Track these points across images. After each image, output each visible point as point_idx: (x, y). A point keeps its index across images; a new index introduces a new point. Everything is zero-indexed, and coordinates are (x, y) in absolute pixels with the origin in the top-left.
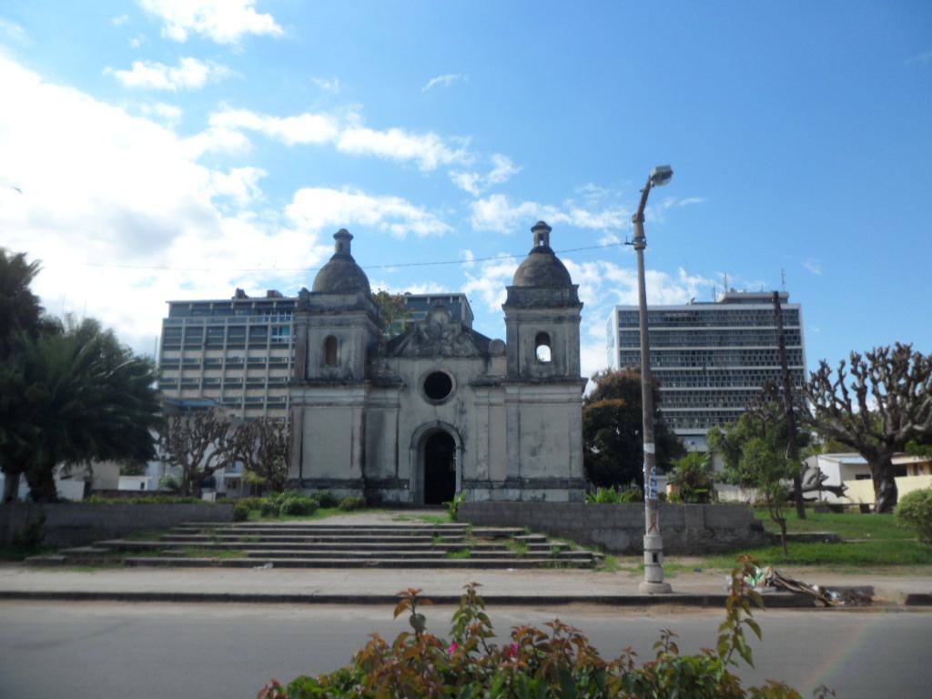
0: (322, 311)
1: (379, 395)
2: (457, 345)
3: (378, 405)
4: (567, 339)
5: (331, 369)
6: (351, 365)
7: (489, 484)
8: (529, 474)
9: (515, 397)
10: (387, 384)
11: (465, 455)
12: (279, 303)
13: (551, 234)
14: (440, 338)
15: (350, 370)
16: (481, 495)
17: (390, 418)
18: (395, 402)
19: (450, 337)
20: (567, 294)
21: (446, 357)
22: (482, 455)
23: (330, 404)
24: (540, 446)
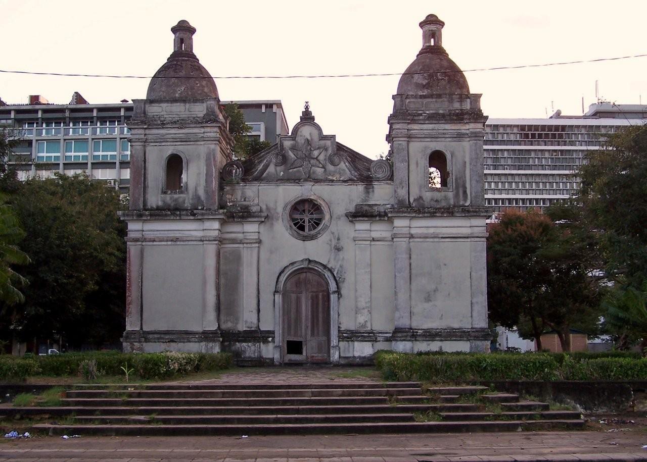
0: (163, 125)
1: (236, 230)
2: (330, 168)
3: (234, 241)
4: (467, 160)
5: (176, 196)
6: (201, 193)
7: (370, 336)
8: (421, 323)
9: (405, 231)
10: (244, 214)
11: (341, 299)
12: (45, 111)
13: (444, 31)
14: (309, 157)
15: (199, 198)
16: (363, 349)
17: (249, 256)
18: (255, 236)
19: (321, 158)
20: (467, 106)
21: (317, 181)
22: (362, 303)
23: (176, 240)
24: (436, 290)
